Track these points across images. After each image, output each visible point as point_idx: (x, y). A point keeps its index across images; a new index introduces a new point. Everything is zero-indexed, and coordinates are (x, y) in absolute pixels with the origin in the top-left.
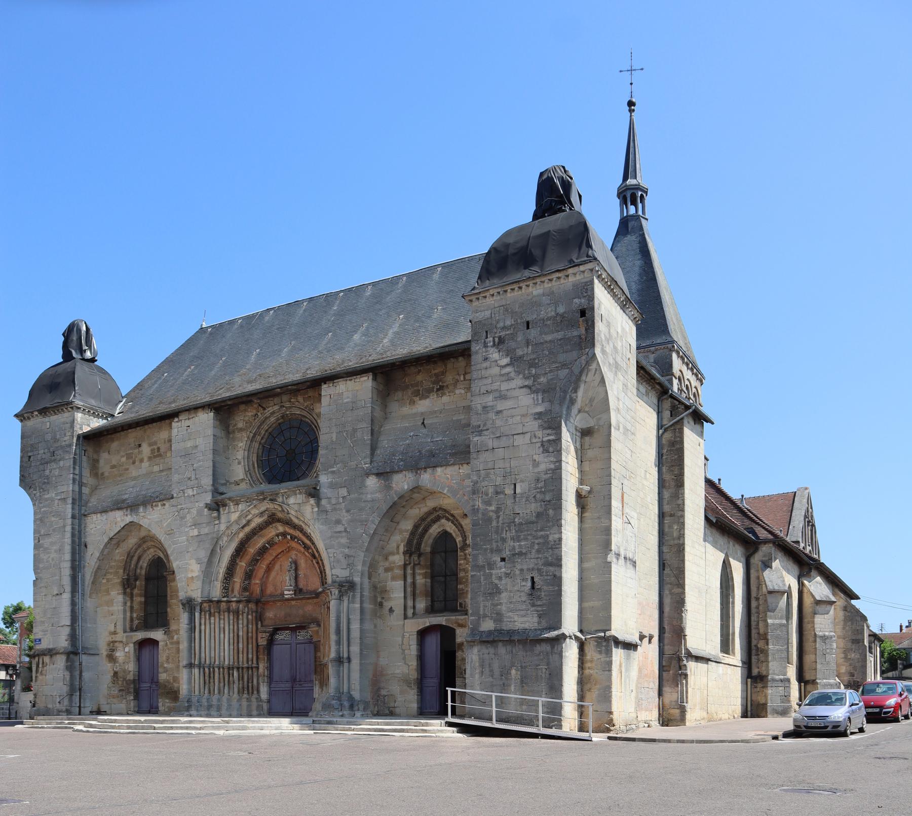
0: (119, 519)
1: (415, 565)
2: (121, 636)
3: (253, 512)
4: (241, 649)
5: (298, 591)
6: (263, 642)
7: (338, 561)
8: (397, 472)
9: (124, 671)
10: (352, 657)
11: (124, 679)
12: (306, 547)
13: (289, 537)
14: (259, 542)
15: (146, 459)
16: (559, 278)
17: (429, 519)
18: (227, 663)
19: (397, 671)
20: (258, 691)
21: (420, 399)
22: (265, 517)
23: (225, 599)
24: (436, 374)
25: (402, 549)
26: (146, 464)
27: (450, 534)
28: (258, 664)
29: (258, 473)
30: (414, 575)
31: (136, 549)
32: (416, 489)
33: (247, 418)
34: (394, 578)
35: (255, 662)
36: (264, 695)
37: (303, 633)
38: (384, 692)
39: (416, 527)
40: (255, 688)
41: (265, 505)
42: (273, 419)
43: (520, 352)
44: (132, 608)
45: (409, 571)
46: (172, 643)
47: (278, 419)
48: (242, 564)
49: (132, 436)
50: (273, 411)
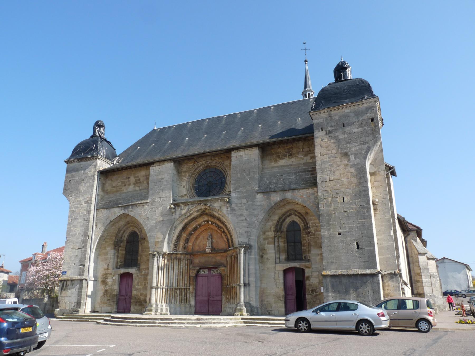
0: (117, 212)
1: (279, 237)
2: (111, 271)
3: (194, 210)
4: (181, 279)
5: (213, 249)
6: (193, 274)
7: (242, 234)
8: (274, 191)
9: (111, 289)
10: (251, 284)
11: (111, 294)
12: (219, 227)
13: (210, 223)
14: (194, 225)
15: (132, 184)
16: (358, 105)
17: (286, 215)
18: (174, 286)
19: (273, 291)
20: (189, 301)
21: (280, 159)
22: (200, 213)
23: (175, 253)
24: (288, 149)
25: (273, 229)
26: (132, 187)
27: (297, 223)
28: (189, 286)
29: (194, 192)
30: (278, 242)
31: (123, 227)
32: (283, 200)
33: (188, 167)
34: (269, 243)
35: (188, 285)
36: (193, 303)
37: (215, 270)
38: (265, 303)
39: (280, 218)
40: (188, 300)
41: (202, 207)
42: (201, 167)
43: (340, 137)
44: (118, 256)
45: (276, 240)
46: (141, 275)
47: (204, 167)
48: (184, 235)
49: (125, 173)
50: (202, 164)
